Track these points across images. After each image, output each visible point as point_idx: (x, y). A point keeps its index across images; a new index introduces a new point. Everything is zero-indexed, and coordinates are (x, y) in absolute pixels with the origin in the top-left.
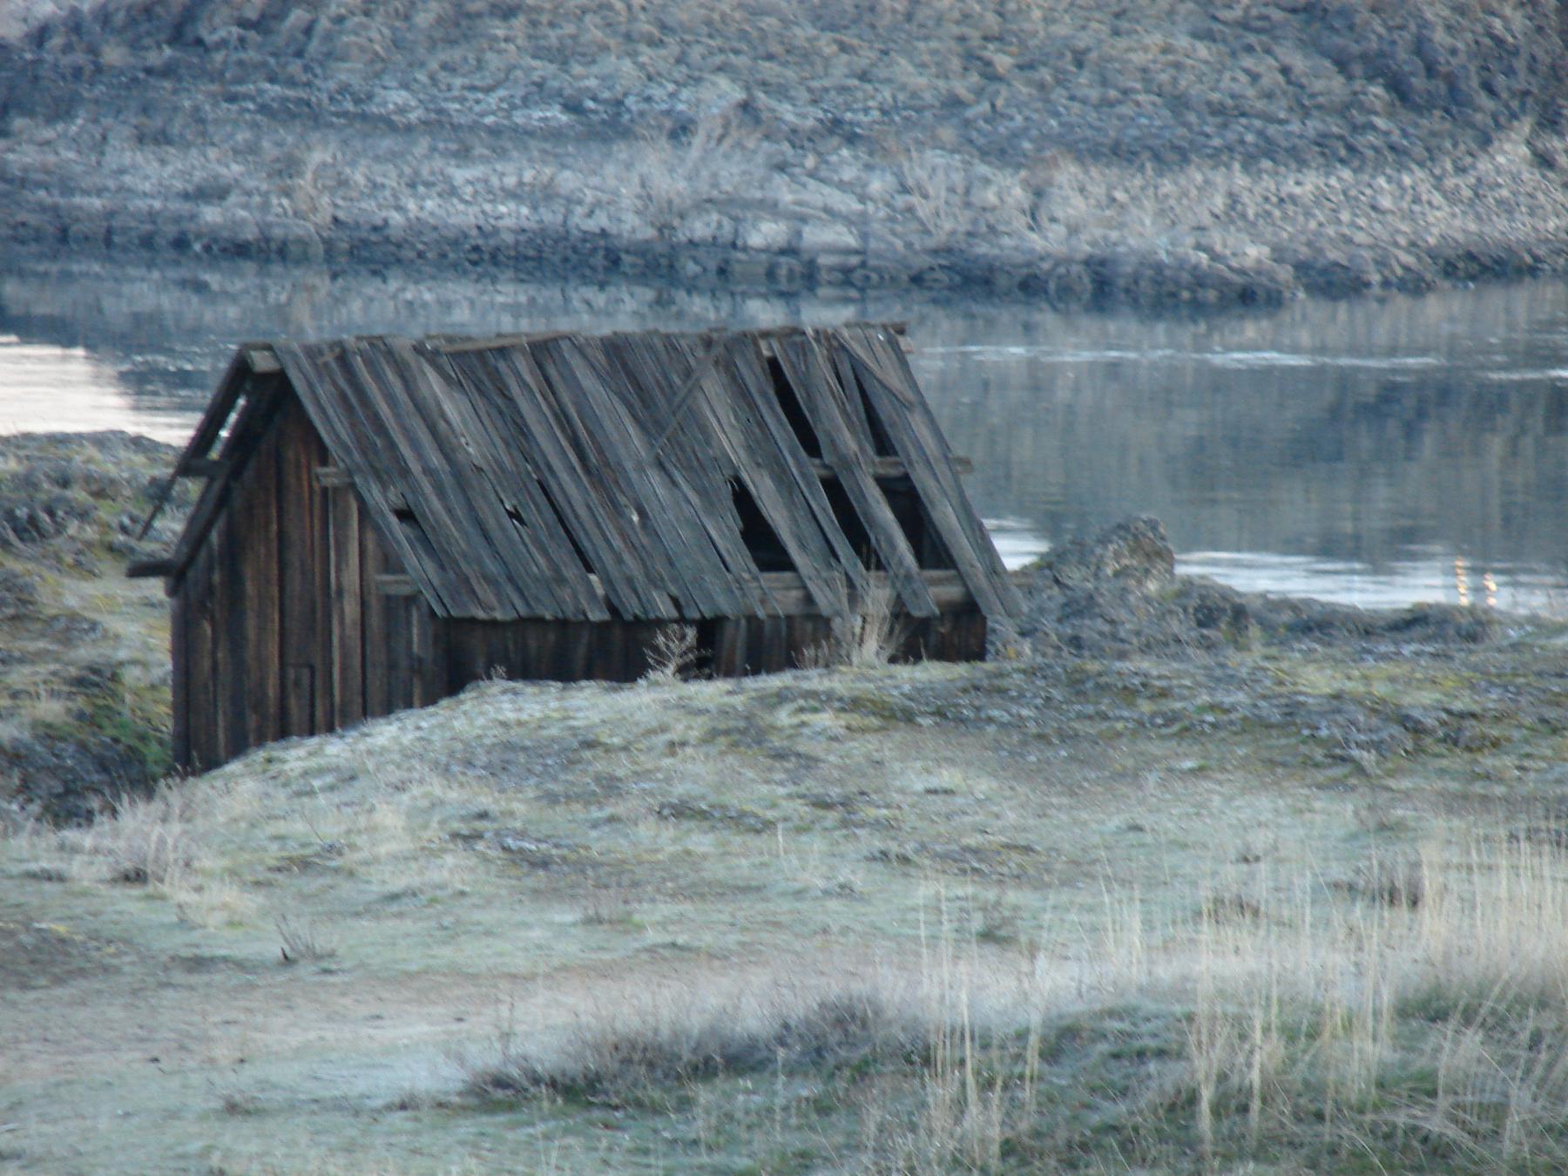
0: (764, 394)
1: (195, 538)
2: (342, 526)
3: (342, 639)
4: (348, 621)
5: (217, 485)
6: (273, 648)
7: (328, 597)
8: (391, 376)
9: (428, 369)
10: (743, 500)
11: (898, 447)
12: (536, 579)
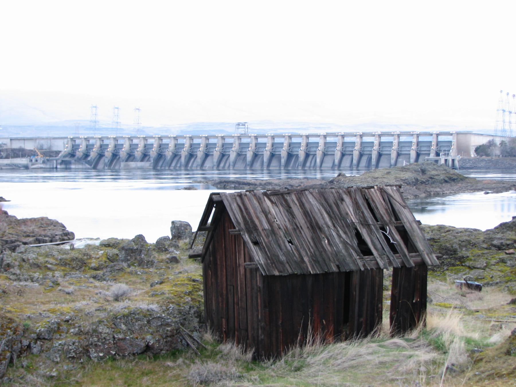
0: (363, 205)
1: (207, 248)
2: (239, 246)
3: (240, 279)
4: (241, 273)
5: (210, 233)
6: (224, 279)
7: (236, 267)
8: (255, 202)
9: (266, 199)
10: (358, 235)
11: (401, 218)
12: (295, 262)
